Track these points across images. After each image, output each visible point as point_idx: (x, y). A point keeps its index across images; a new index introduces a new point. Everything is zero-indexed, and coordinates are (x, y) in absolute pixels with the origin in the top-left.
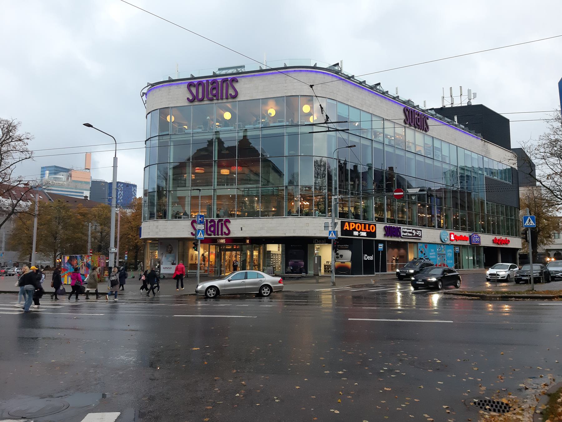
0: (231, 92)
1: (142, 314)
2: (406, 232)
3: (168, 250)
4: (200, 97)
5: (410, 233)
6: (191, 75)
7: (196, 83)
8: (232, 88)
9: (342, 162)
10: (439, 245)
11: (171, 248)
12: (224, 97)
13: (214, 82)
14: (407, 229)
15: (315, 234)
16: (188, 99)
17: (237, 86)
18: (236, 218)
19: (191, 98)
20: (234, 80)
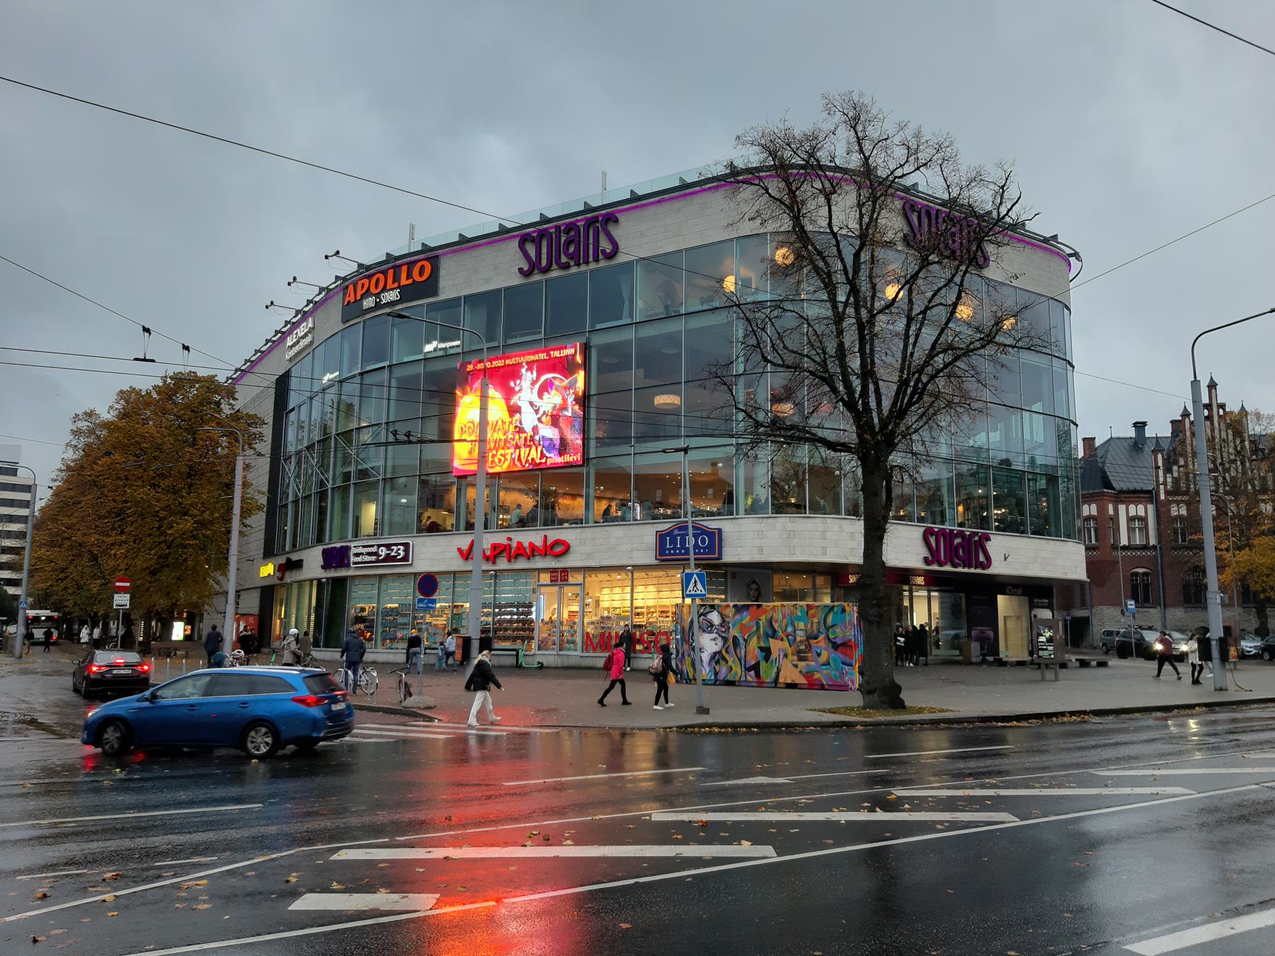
0: (605, 245)
1: (906, 780)
2: (362, 554)
3: (751, 593)
4: (544, 263)
5: (370, 554)
6: (460, 235)
7: (535, 235)
8: (606, 237)
9: (64, 468)
10: (531, 574)
11: (756, 589)
12: (591, 259)
13: (570, 227)
14: (364, 547)
15: (824, 551)
16: (521, 270)
17: (616, 232)
18: (808, 515)
19: (526, 267)
20: (611, 219)
